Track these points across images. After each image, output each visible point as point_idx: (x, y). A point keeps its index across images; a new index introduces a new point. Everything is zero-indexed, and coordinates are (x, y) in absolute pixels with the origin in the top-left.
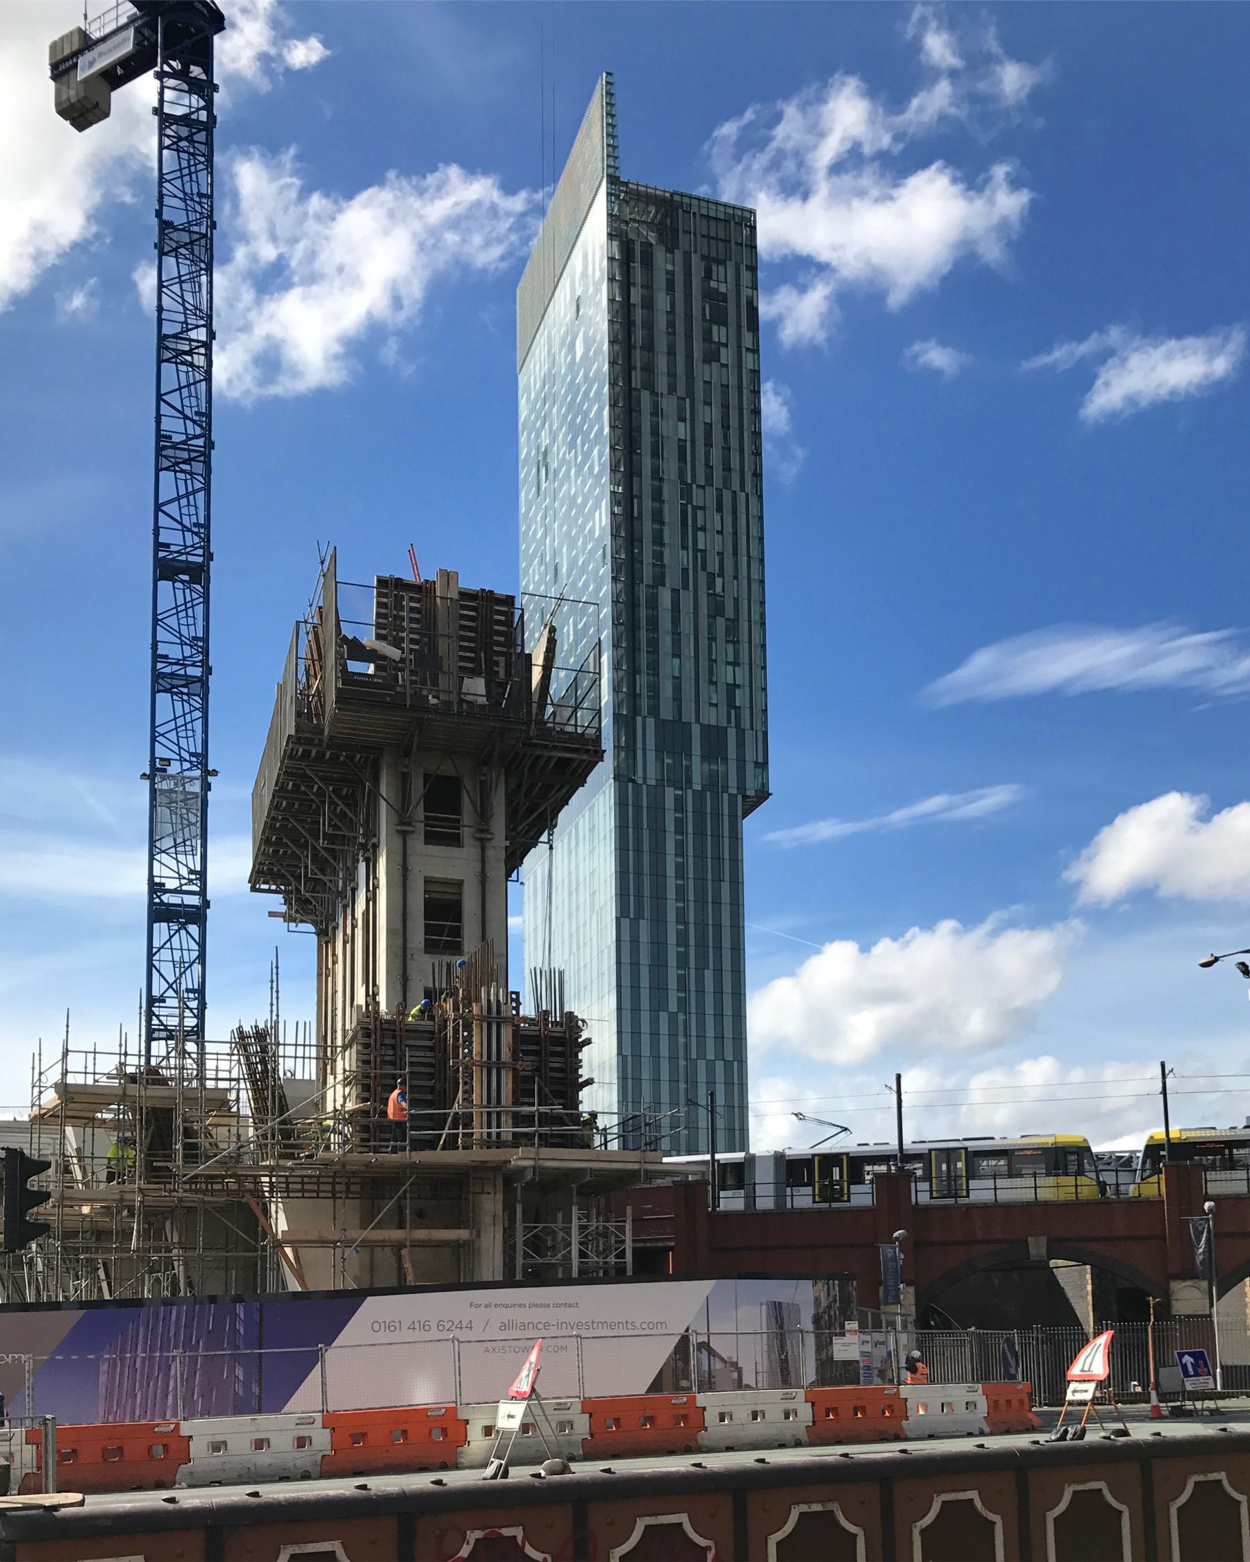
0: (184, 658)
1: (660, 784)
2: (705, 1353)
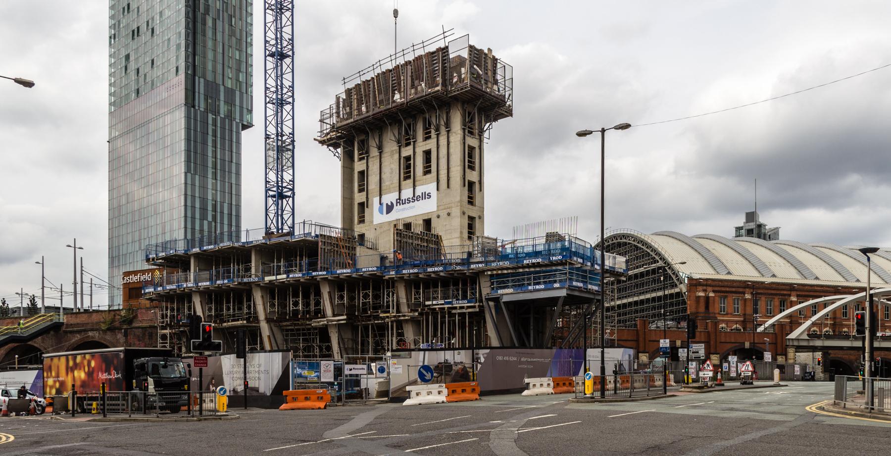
1: (206, 111)
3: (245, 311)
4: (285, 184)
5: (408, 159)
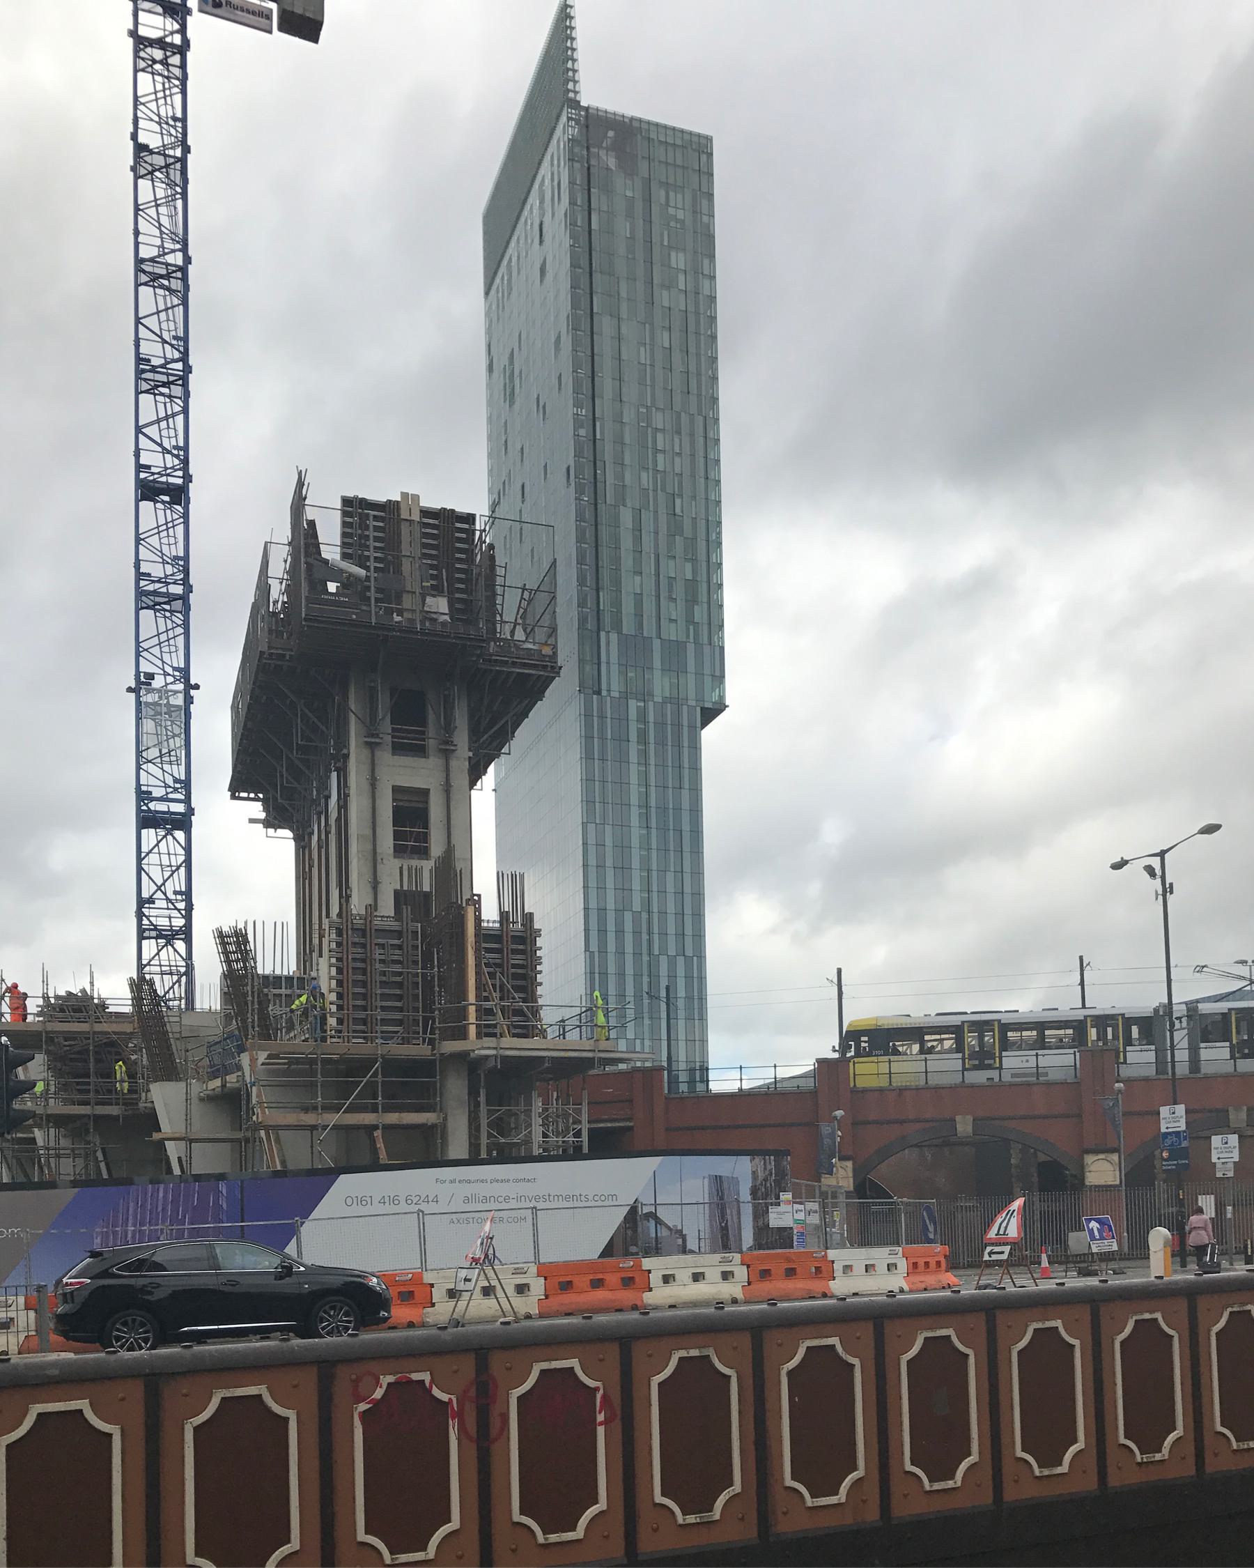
0: (166, 576)
1: (625, 696)
2: (652, 1223)
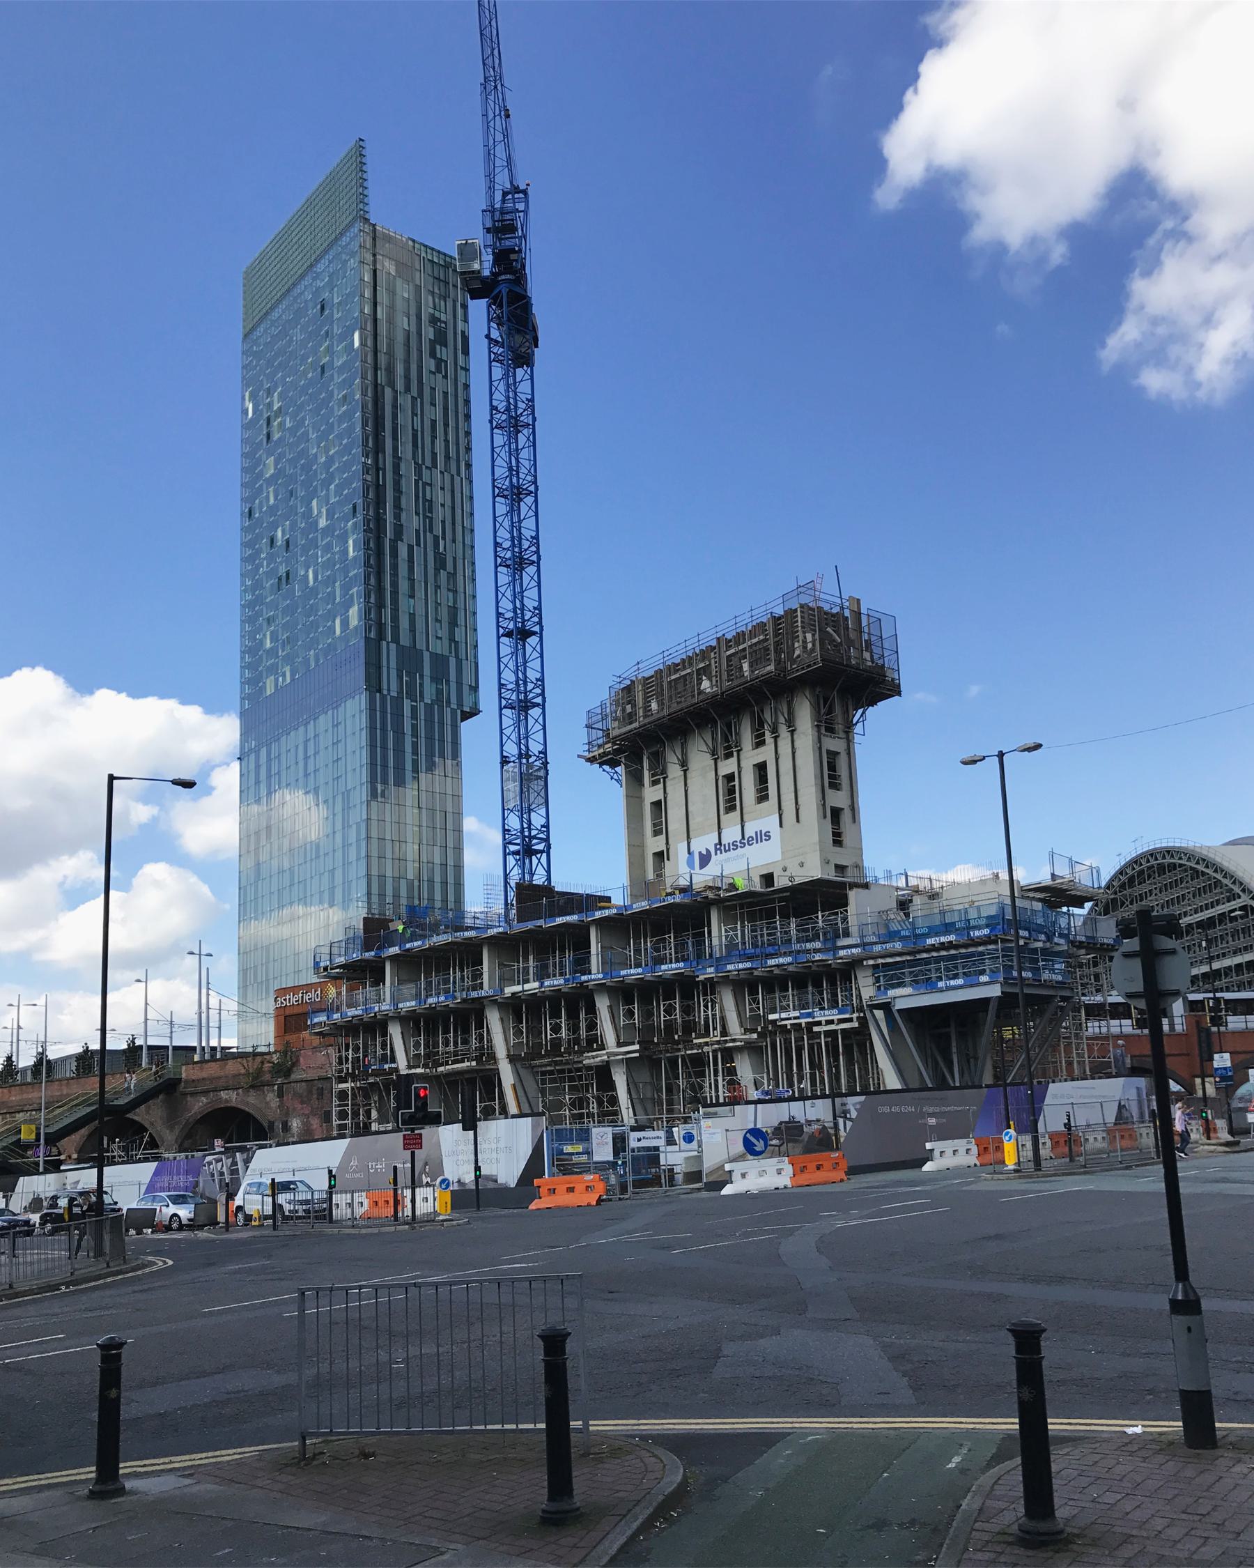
3: (474, 1043)
4: (534, 833)
5: (730, 778)
